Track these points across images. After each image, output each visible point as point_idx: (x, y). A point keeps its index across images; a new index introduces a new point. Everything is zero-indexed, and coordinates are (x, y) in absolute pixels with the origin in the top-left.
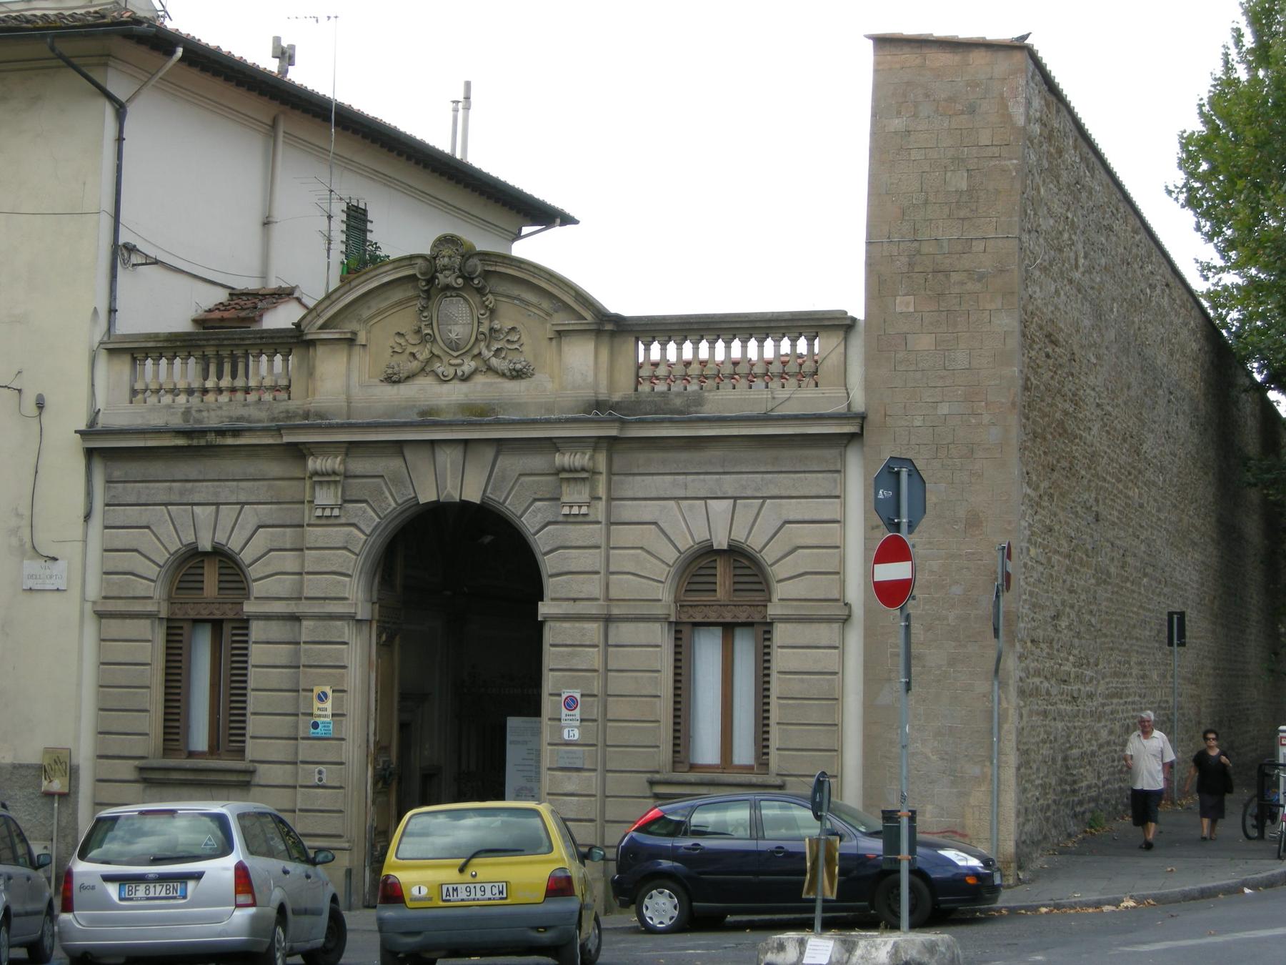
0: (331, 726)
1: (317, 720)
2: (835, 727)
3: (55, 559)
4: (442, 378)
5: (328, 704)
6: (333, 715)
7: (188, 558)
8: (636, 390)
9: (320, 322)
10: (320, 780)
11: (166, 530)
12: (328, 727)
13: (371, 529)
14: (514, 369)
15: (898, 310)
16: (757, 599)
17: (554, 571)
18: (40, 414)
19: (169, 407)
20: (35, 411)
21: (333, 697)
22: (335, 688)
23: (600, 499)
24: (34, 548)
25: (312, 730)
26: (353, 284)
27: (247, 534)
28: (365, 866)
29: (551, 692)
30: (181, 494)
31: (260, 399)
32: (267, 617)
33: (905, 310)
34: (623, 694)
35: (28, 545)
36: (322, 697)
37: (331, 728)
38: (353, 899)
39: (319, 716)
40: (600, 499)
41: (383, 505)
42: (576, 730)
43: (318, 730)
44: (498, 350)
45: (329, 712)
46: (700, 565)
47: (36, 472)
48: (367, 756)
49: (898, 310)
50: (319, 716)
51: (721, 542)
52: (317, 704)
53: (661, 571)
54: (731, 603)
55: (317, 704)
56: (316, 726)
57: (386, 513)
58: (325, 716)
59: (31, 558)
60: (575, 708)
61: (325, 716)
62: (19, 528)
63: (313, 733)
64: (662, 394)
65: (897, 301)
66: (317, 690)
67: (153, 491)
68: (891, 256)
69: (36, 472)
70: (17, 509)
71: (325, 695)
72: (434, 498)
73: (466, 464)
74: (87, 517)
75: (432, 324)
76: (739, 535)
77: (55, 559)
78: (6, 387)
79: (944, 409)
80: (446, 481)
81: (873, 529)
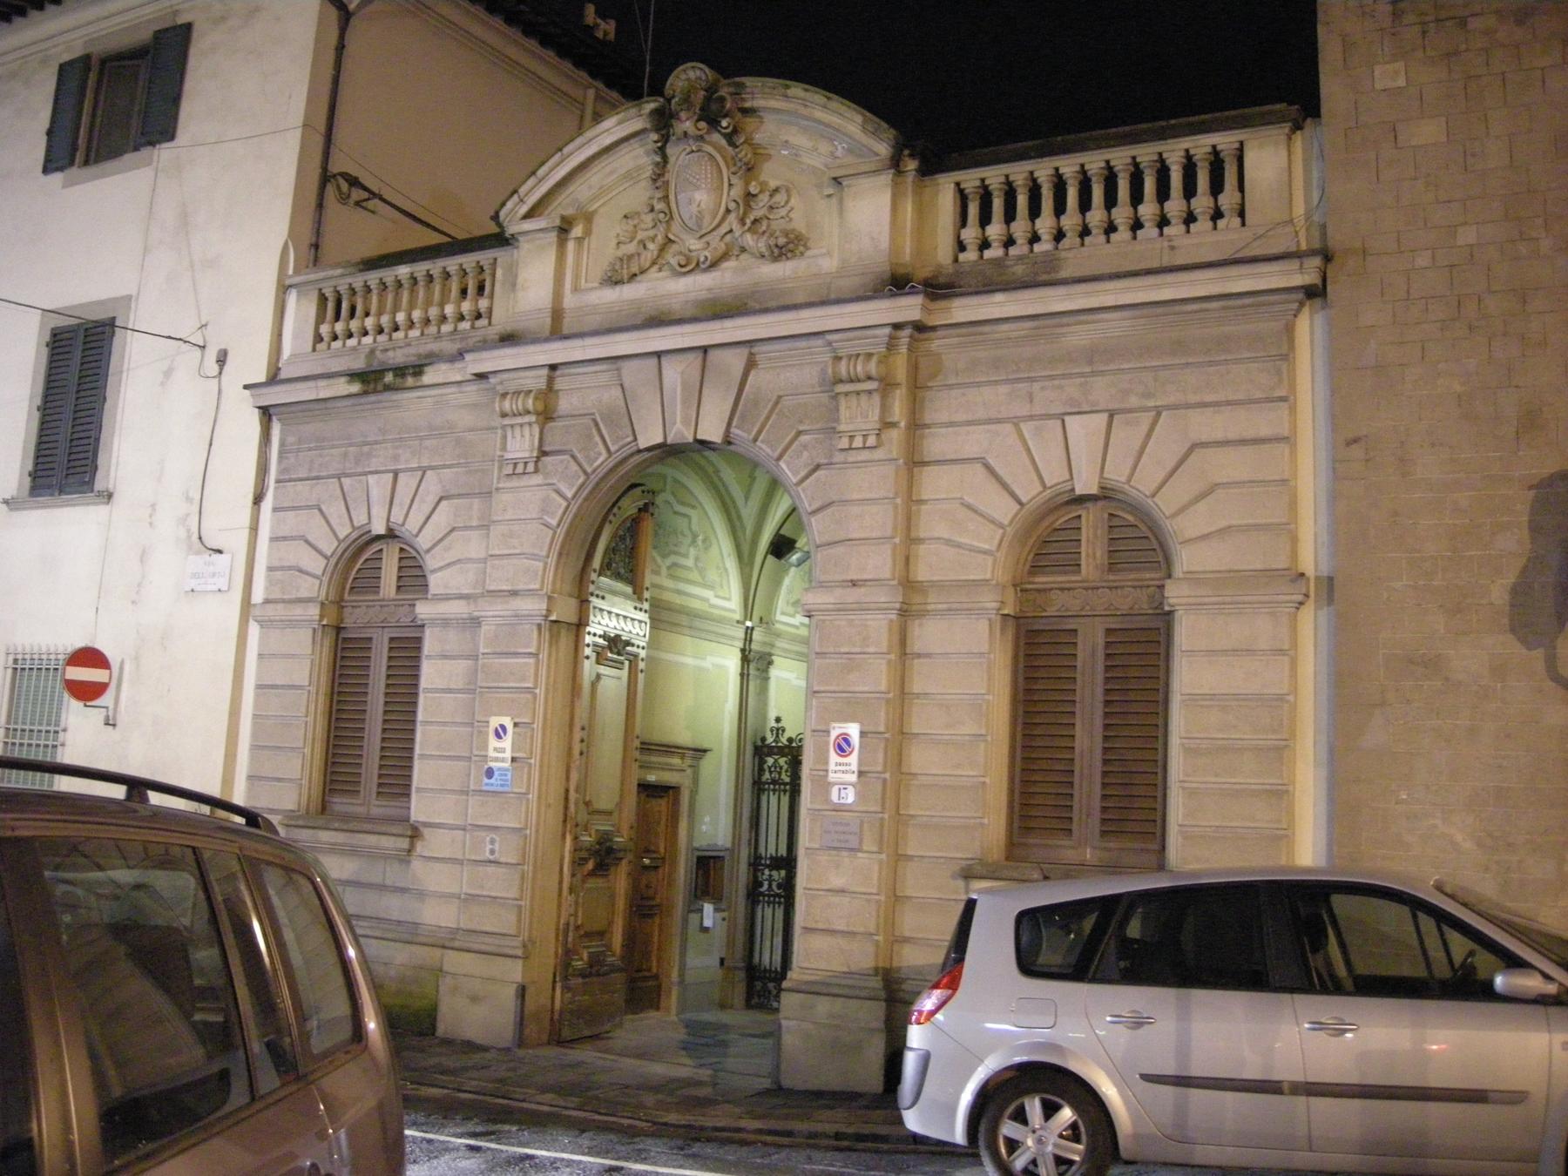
0: (509, 774)
1: (492, 764)
2: (1281, 795)
3: (220, 552)
4: (684, 270)
5: (507, 743)
6: (513, 760)
7: (713, 620)
8: (956, 260)
9: (524, 209)
10: (492, 852)
11: (336, 511)
12: (506, 775)
13: (574, 489)
14: (777, 246)
15: (1378, 86)
16: (1148, 576)
17: (827, 538)
18: (220, 373)
19: (354, 349)
20: (216, 368)
21: (514, 733)
22: (517, 720)
23: (893, 425)
24: (200, 538)
25: (486, 780)
26: (566, 150)
27: (427, 509)
28: (554, 982)
29: (813, 728)
30: (357, 462)
31: (455, 330)
32: (445, 622)
33: (1391, 84)
34: (225, 707)
35: (196, 536)
36: (500, 733)
37: (509, 777)
38: (527, 1031)
39: (496, 760)
40: (893, 425)
41: (592, 454)
42: (850, 788)
43: (492, 781)
44: (756, 221)
45: (508, 755)
46: (1057, 525)
47: (211, 445)
48: (565, 821)
49: (1378, 86)
50: (496, 760)
51: (1086, 484)
52: (493, 742)
53: (987, 538)
54: (1104, 584)
55: (493, 742)
56: (490, 773)
57: (596, 464)
58: (503, 760)
59: (198, 553)
60: (851, 753)
61: (503, 760)
62: (188, 515)
63: (487, 784)
64: (996, 262)
65: (1377, 73)
66: (495, 722)
67: (327, 459)
68: (1361, 7)
69: (211, 445)
70: (187, 492)
71: (503, 727)
72: (659, 440)
73: (705, 391)
74: (258, 499)
75: (667, 197)
76: (1117, 473)
77: (220, 552)
78: (180, 339)
79: (1467, 236)
80: (675, 413)
81: (1348, 444)
